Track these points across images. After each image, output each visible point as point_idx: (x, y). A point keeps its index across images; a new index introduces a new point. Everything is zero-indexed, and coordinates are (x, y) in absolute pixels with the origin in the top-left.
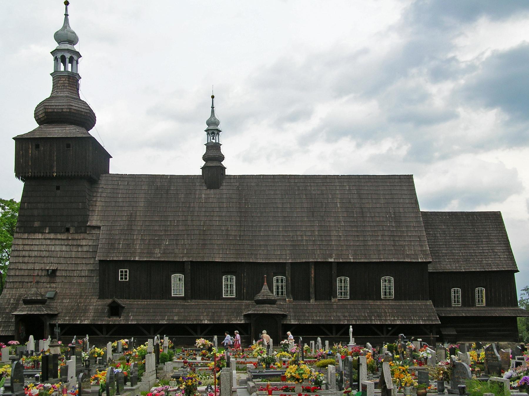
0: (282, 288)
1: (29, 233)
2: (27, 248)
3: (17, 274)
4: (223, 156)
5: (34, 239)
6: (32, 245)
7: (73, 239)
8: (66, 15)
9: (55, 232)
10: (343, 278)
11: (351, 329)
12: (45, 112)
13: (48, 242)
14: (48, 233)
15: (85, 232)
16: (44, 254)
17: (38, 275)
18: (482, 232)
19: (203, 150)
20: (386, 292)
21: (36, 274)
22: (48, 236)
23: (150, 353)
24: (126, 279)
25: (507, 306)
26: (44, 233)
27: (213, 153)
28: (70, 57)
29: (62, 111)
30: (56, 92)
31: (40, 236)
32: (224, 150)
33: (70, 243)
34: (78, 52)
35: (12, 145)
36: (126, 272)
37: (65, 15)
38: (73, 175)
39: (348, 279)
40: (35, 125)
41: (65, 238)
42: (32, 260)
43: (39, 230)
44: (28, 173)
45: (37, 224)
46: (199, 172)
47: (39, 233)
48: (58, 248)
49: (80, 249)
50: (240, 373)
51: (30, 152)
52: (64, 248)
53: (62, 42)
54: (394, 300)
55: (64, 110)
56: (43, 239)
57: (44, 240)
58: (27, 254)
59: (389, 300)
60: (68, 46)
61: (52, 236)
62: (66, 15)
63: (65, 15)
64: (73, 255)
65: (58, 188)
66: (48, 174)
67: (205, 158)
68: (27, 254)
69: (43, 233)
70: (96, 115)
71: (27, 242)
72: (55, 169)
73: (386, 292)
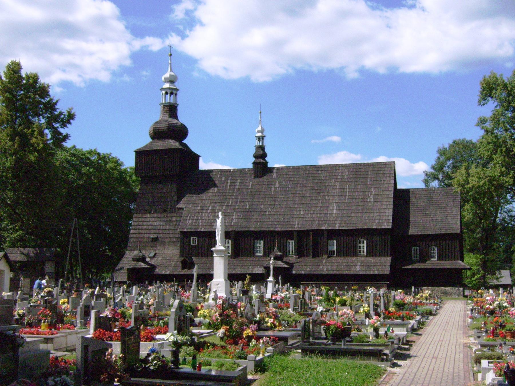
0: (360, 251)
2: (141, 223)
13: (153, 219)
16: (150, 227)
18: (173, 232)
19: (253, 151)
20: (260, 248)
22: (152, 215)
24: (196, 243)
25: (344, 256)
31: (148, 215)
32: (267, 150)
33: (166, 219)
35: (134, 154)
36: (196, 239)
40: (150, 140)
42: (144, 231)
46: (251, 166)
48: (158, 223)
50: (375, 345)
52: (162, 223)
58: (140, 227)
59: (362, 256)
61: (155, 215)
64: (167, 227)
71: (140, 219)
73: (260, 248)
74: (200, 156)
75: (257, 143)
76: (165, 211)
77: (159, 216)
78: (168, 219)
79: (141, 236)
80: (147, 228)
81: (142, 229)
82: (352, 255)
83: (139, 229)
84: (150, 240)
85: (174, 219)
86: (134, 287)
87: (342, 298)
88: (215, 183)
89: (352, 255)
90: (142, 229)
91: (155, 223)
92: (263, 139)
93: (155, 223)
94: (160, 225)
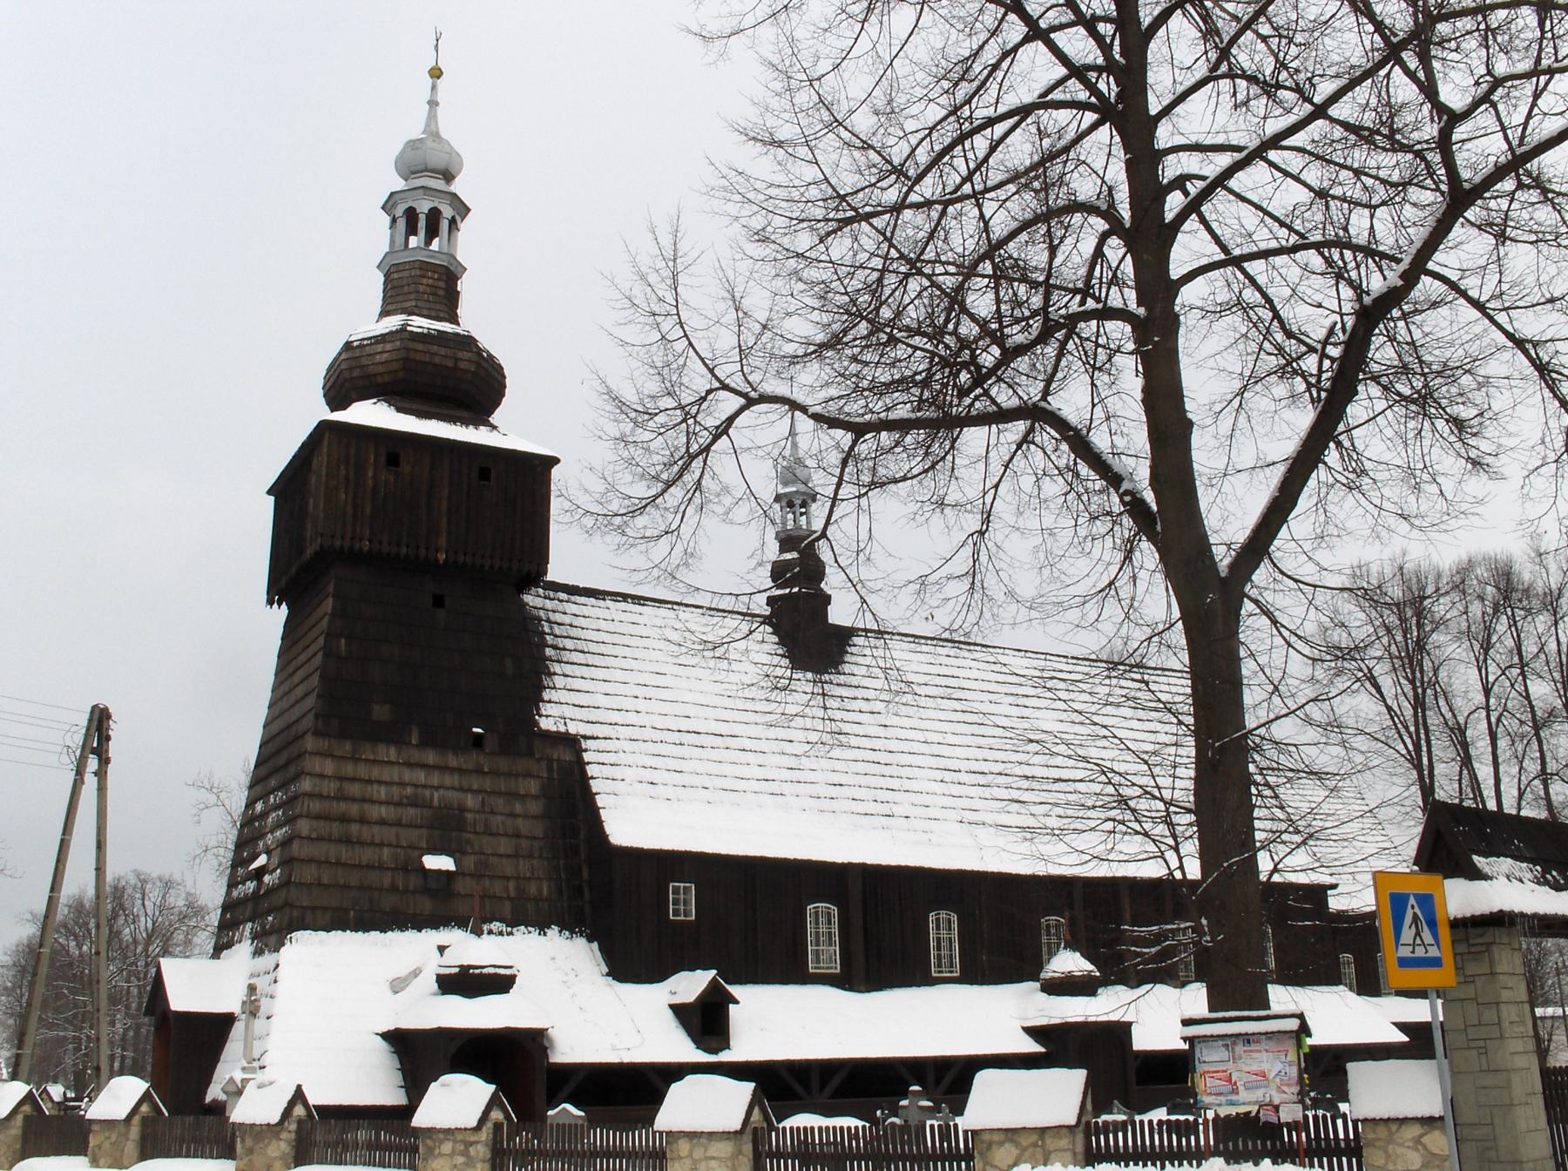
2: (355, 789)
3: (325, 880)
5: (374, 761)
7: (494, 773)
8: (433, 104)
10: (943, 914)
11: (1191, 1118)
12: (406, 360)
15: (530, 754)
17: (394, 889)
22: (416, 755)
26: (406, 744)
28: (431, 210)
29: (456, 368)
34: (392, 194)
37: (429, 103)
38: (496, 568)
39: (955, 918)
41: (470, 766)
43: (389, 734)
44: (361, 540)
47: (389, 741)
49: (518, 808)
51: (370, 474)
53: (432, 171)
54: (1541, 1071)
55: (462, 365)
58: (354, 809)
60: (439, 184)
61: (431, 757)
62: (433, 104)
63: (429, 103)
65: (438, 601)
66: (422, 552)
68: (354, 809)
71: (349, 769)
72: (443, 541)
81: (363, 821)
83: (345, 819)
90: (363, 821)
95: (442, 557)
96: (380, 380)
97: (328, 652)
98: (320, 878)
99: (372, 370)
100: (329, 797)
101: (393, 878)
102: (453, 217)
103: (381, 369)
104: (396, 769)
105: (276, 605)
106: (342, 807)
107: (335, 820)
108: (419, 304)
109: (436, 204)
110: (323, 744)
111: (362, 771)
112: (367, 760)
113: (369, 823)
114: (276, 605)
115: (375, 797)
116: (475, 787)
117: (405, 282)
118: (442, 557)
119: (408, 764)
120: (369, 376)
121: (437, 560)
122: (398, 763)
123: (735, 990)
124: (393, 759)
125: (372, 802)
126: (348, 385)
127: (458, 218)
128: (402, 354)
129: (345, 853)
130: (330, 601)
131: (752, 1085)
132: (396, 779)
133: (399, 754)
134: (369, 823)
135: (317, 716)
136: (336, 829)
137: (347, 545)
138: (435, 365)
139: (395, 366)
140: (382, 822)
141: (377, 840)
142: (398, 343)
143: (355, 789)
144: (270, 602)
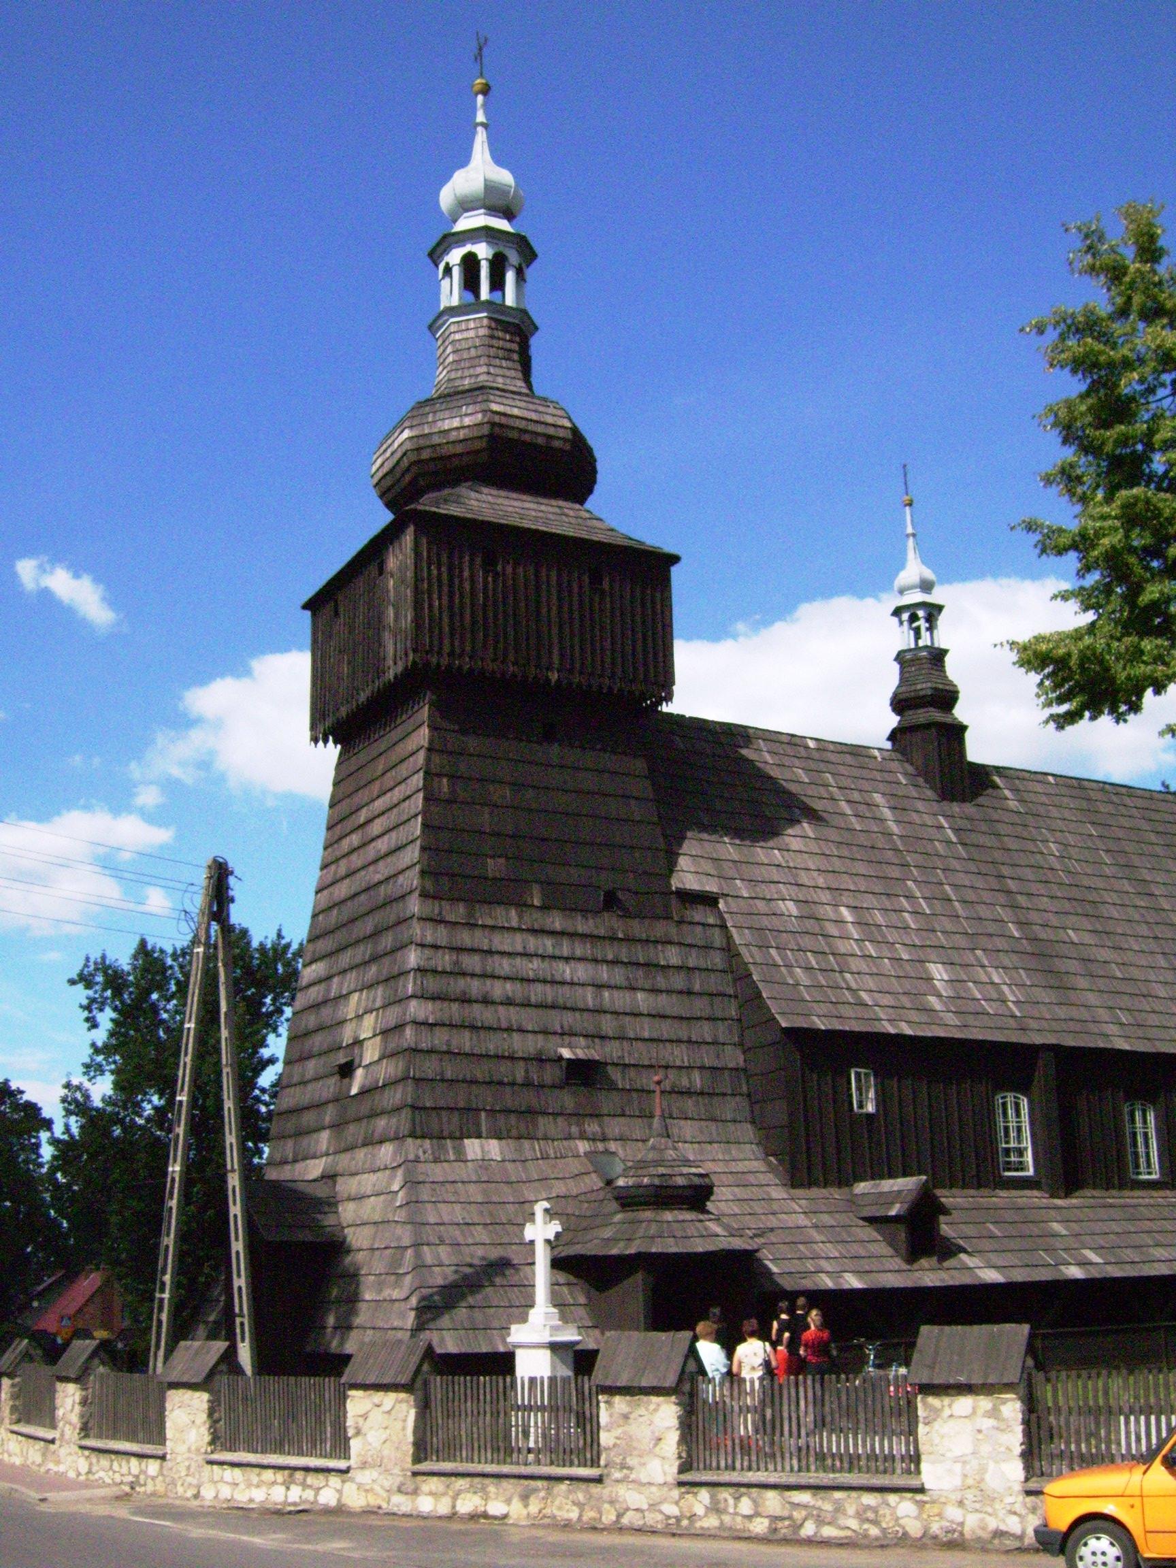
1: (471, 900)
2: (472, 962)
4: (951, 688)
5: (493, 928)
6: (490, 952)
9: (570, 909)
14: (541, 908)
17: (528, 1084)
19: (890, 679)
21: (520, 1076)
22: (535, 919)
23: (718, 1057)
26: (525, 905)
27: (924, 687)
30: (454, 352)
32: (954, 669)
39: (1024, 1103)
45: (494, 867)
48: (582, 972)
52: (604, 973)
56: (528, 930)
57: (605, 967)
58: (475, 987)
61: (556, 921)
66: (533, 671)
67: (899, 704)
69: (522, 906)
70: (596, 487)
71: (466, 938)
74: (674, 559)
75: (900, 638)
76: (611, 902)
77: (581, 928)
78: (641, 956)
79: (493, 1044)
80: (519, 998)
81: (486, 1001)
82: (818, 1173)
83: (465, 1000)
84: (551, 1074)
85: (672, 956)
86: (26, 1341)
87: (206, 1323)
88: (347, 1063)
89: (818, 1173)
90: (486, 1001)
91: (566, 971)
92: (931, 619)
93: (566, 971)
94: (599, 986)
95: (554, 676)
96: (456, 462)
97: (430, 798)
98: (442, 1073)
99: (444, 451)
100: (444, 972)
101: (527, 1071)
102: (520, 265)
103: (459, 449)
104: (519, 937)
105: (321, 743)
106: (462, 983)
107: (455, 1000)
108: (492, 370)
109: (501, 249)
110: (433, 908)
111: (480, 939)
112: (484, 926)
113: (493, 1003)
114: (321, 743)
115: (498, 972)
116: (610, 957)
117: (470, 343)
118: (554, 676)
119: (534, 931)
120: (441, 458)
121: (548, 680)
122: (520, 929)
123: (948, 1197)
124: (514, 924)
125: (493, 977)
126: (414, 469)
127: (524, 266)
128: (486, 430)
129: (465, 1041)
130: (425, 731)
131: (1025, 1328)
132: (519, 949)
133: (520, 917)
134: (493, 1003)
135: (423, 873)
136: (454, 1011)
137: (445, 661)
138: (524, 443)
139: (478, 445)
140: (509, 1002)
141: (504, 1025)
142: (480, 416)
143: (472, 962)
144: (315, 740)
